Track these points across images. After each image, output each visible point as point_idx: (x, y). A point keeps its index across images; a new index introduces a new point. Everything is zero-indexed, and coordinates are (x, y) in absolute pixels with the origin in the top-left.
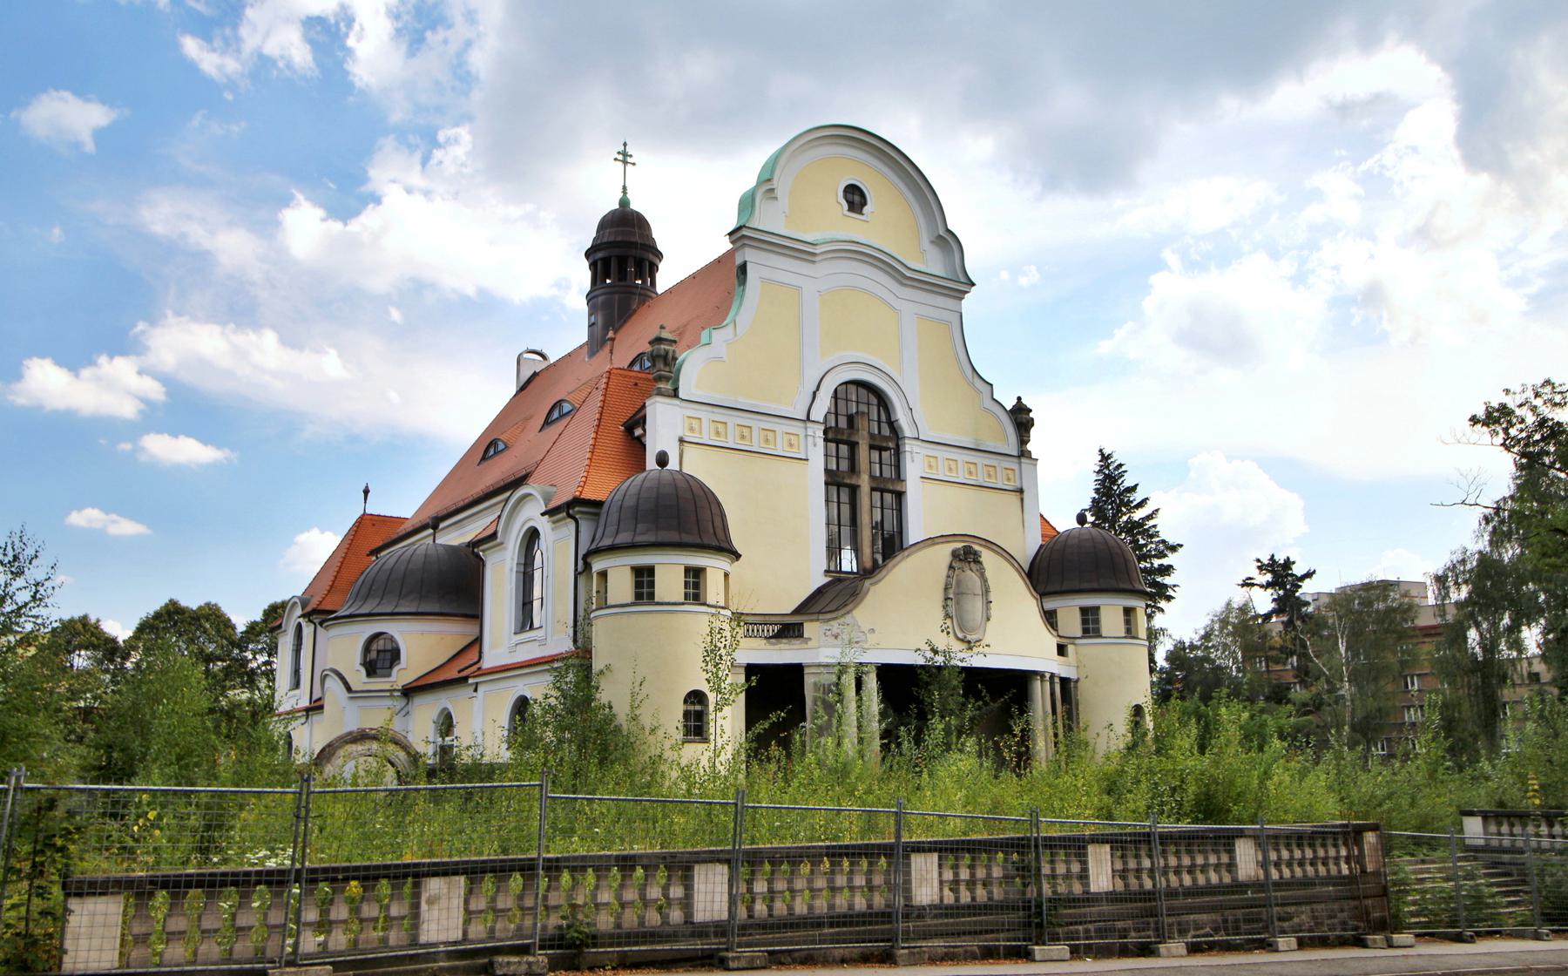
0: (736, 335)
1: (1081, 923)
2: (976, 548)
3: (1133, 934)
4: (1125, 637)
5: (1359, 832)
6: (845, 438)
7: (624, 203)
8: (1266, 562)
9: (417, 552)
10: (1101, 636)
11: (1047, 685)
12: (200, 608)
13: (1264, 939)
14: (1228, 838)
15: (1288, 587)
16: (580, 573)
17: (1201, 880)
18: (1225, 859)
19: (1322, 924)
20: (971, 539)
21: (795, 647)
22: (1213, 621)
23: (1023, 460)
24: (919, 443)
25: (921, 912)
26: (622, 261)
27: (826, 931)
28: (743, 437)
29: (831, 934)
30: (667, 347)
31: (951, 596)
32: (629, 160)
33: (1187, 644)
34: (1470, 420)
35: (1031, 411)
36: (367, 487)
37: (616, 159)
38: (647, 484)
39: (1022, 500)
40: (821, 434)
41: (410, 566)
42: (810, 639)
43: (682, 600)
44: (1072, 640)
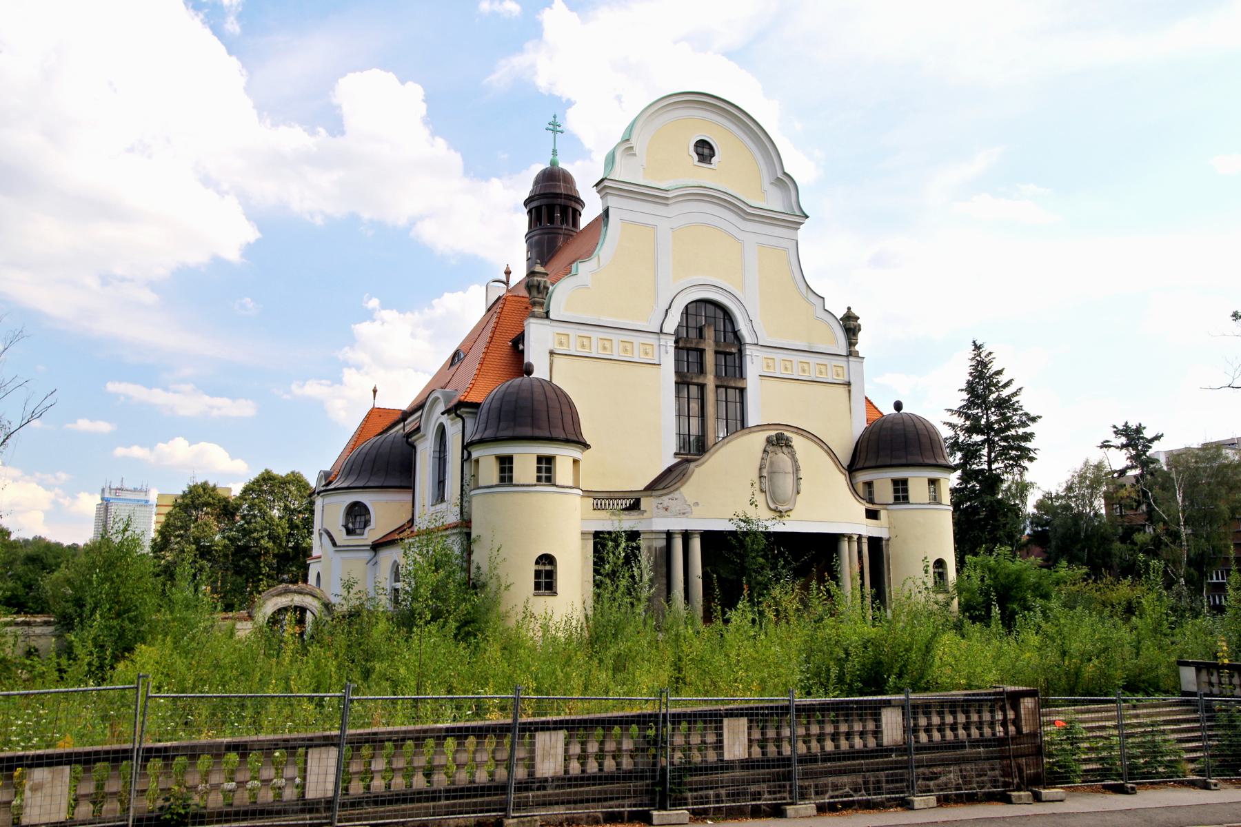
0: (599, 265)
1: (712, 788)
2: (788, 434)
3: (766, 796)
4: (929, 504)
5: (1015, 698)
6: (693, 346)
7: (553, 163)
8: (1121, 428)
9: (387, 439)
10: (909, 503)
11: (855, 545)
12: (287, 476)
13: (905, 797)
14: (875, 708)
15: (1140, 448)
16: (466, 460)
17: (844, 745)
18: (871, 726)
19: (970, 782)
21: (633, 517)
22: (1073, 476)
23: (851, 359)
24: (758, 348)
25: (543, 783)
26: (551, 209)
28: (605, 348)
29: (447, 806)
30: (539, 279)
31: (765, 474)
33: (1054, 495)
34: (1233, 316)
38: (510, 390)
39: (849, 391)
41: (381, 450)
42: (645, 511)
43: (535, 482)
44: (885, 506)
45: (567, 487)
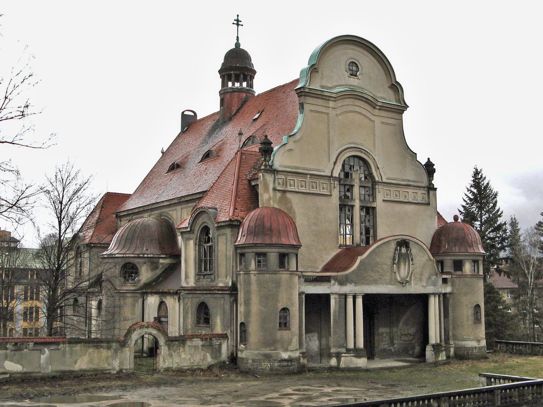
7: (237, 45)
35: (434, 165)
37: (233, 23)
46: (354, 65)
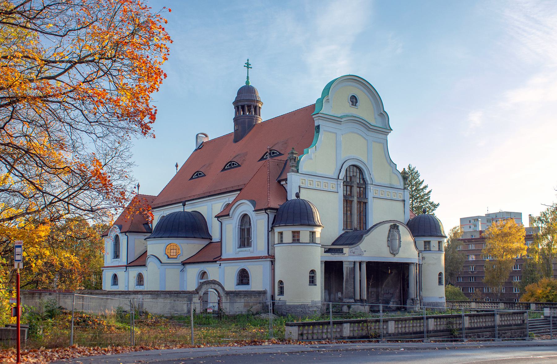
2: (398, 224)
7: (247, 82)
16: (270, 231)
20: (396, 222)
23: (405, 190)
24: (373, 186)
27: (412, 335)
32: (250, 66)
36: (139, 184)
40: (342, 184)
42: (345, 254)
45: (306, 243)
46: (354, 98)
